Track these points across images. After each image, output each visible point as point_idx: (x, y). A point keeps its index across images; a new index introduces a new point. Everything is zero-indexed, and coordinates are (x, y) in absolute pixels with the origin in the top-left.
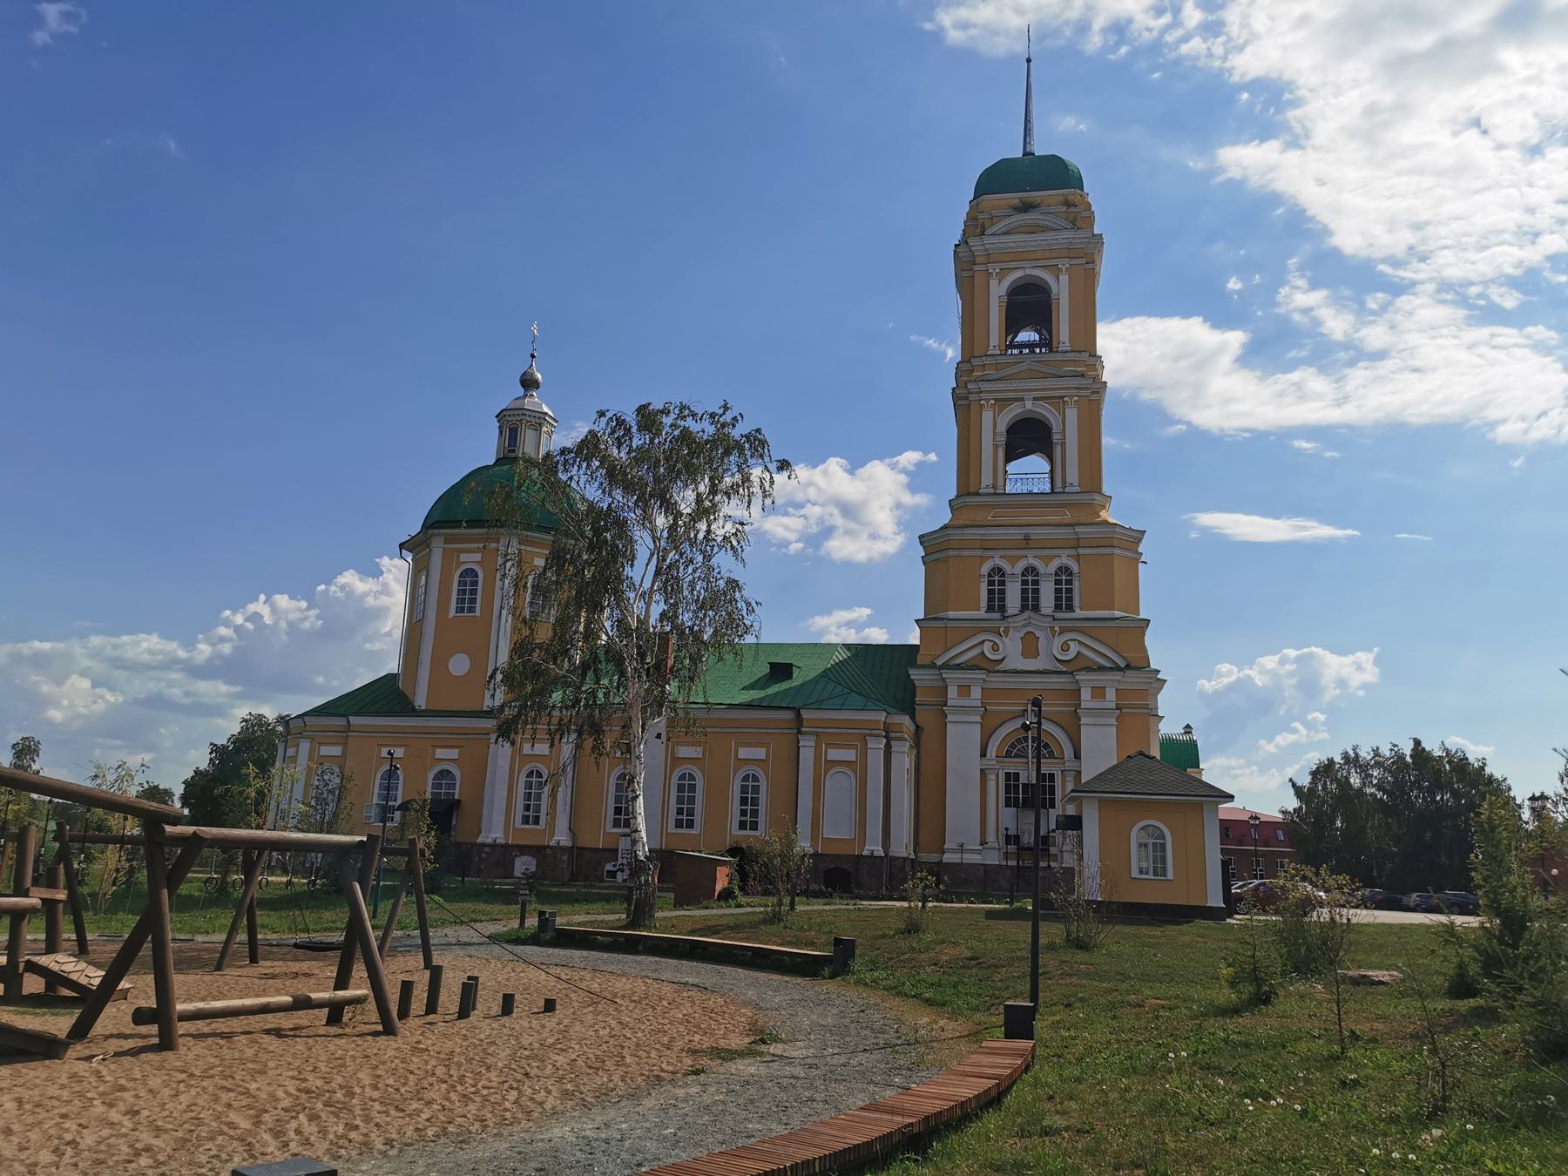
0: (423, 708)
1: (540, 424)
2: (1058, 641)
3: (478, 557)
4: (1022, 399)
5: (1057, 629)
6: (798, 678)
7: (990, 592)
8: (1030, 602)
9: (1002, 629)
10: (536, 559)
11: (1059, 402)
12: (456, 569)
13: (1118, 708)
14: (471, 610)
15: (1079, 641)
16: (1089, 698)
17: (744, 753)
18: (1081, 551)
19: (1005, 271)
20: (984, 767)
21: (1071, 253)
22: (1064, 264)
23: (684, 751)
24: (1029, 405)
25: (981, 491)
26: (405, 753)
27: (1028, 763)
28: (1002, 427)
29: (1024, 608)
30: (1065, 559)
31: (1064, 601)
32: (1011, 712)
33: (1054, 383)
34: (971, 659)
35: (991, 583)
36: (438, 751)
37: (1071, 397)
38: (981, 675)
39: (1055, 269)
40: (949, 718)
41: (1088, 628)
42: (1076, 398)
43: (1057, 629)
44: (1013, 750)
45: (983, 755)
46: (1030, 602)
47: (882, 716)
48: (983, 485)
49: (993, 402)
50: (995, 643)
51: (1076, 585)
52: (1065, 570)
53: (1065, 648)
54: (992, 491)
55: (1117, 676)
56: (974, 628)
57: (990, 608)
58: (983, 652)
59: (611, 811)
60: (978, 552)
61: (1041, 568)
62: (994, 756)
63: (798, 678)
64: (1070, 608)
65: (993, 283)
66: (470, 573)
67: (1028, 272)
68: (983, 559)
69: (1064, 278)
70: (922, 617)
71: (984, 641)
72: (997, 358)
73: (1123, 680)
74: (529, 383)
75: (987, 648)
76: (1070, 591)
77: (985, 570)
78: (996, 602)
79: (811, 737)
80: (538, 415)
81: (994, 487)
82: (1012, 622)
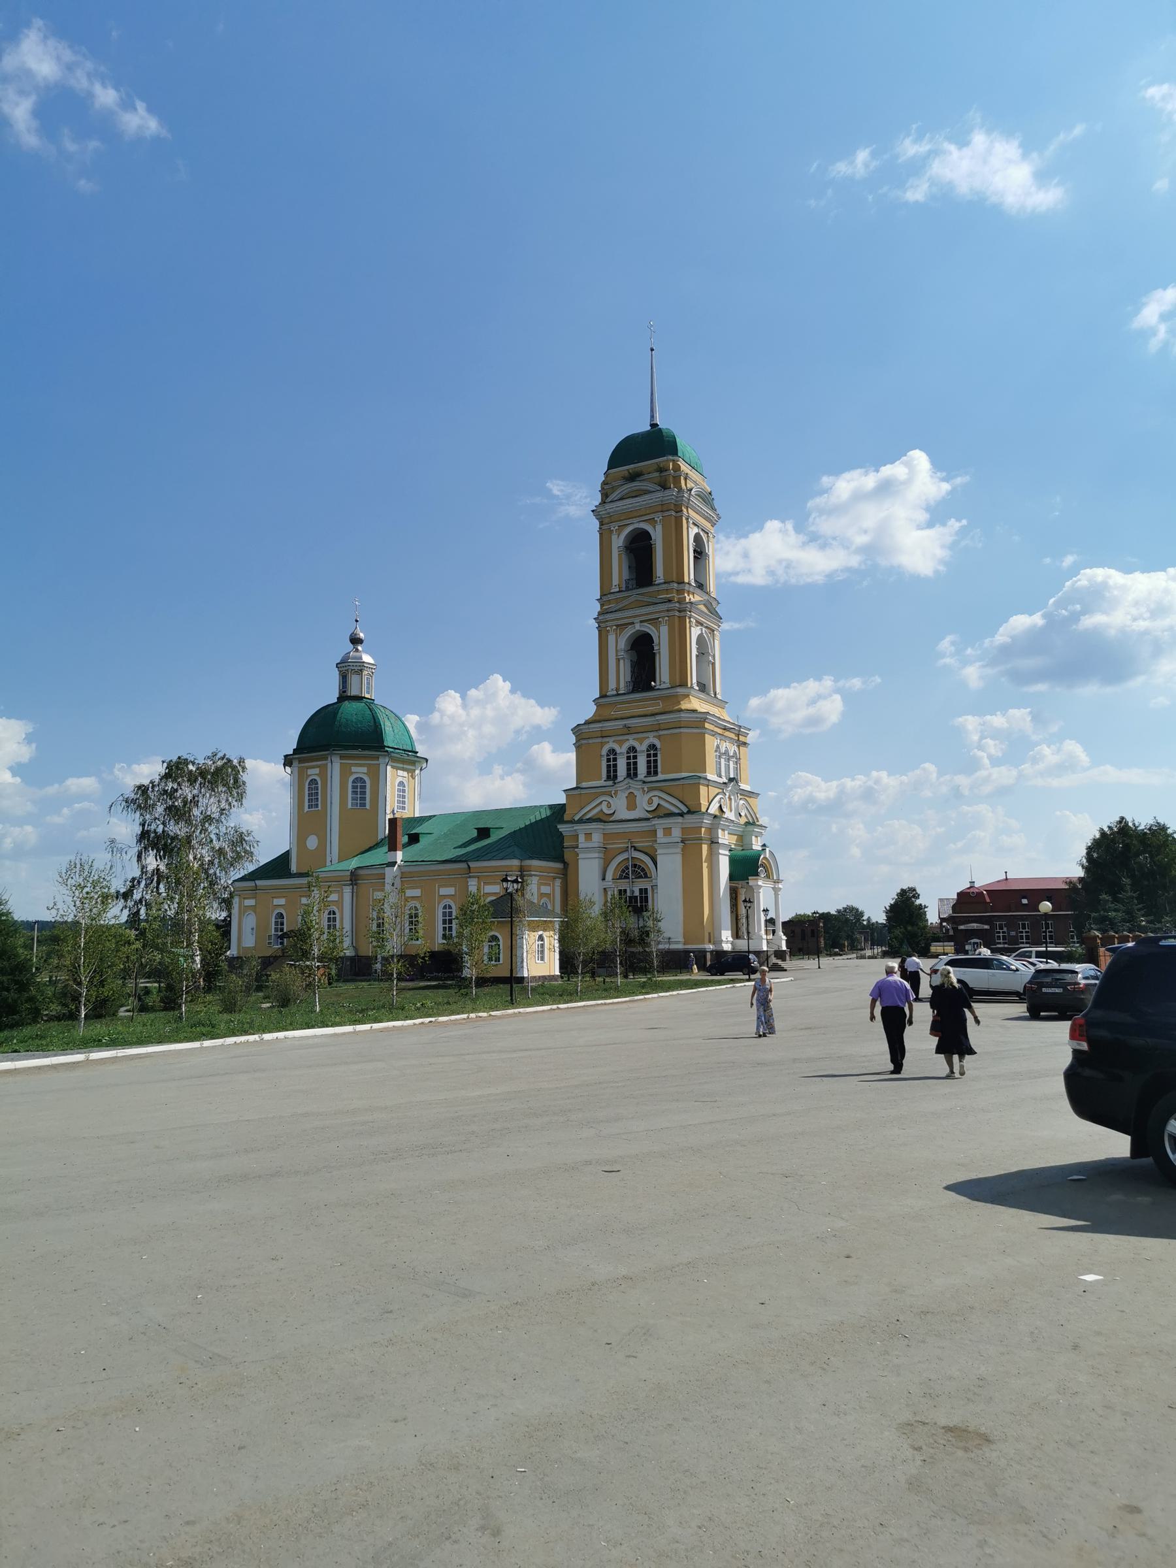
0: (295, 872)
1: (361, 670)
2: (647, 797)
3: (365, 770)
4: (633, 623)
5: (646, 789)
6: (494, 837)
7: (609, 766)
8: (632, 772)
9: (613, 792)
10: (352, 768)
11: (655, 621)
12: (307, 778)
13: (682, 842)
14: (317, 806)
15: (659, 797)
16: (662, 836)
17: (444, 891)
18: (661, 733)
19: (622, 527)
20: (605, 887)
21: (663, 508)
22: (658, 517)
23: (410, 893)
24: (638, 627)
25: (608, 694)
26: (286, 902)
27: (629, 882)
28: (622, 644)
29: (629, 775)
30: (651, 739)
31: (652, 769)
32: (621, 848)
33: (651, 609)
34: (595, 815)
35: (608, 760)
36: (275, 900)
37: (663, 617)
38: (600, 826)
39: (652, 521)
40: (581, 856)
41: (666, 788)
42: (667, 618)
43: (646, 789)
44: (624, 875)
45: (604, 879)
46: (632, 772)
47: (516, 863)
48: (610, 690)
49: (615, 627)
50: (609, 802)
51: (659, 758)
52: (653, 747)
53: (650, 802)
54: (615, 692)
55: (680, 819)
56: (598, 792)
57: (609, 778)
58: (602, 810)
59: (441, 922)
60: (599, 740)
61: (618, 750)
62: (611, 878)
63: (494, 837)
64: (656, 773)
65: (614, 537)
66: (313, 781)
67: (636, 526)
68: (602, 744)
69: (659, 527)
70: (575, 786)
71: (601, 802)
72: (616, 594)
73: (685, 821)
74: (355, 641)
75: (604, 807)
76: (656, 761)
77: (604, 752)
78: (612, 775)
79: (474, 879)
80: (360, 664)
81: (617, 689)
82: (619, 787)
